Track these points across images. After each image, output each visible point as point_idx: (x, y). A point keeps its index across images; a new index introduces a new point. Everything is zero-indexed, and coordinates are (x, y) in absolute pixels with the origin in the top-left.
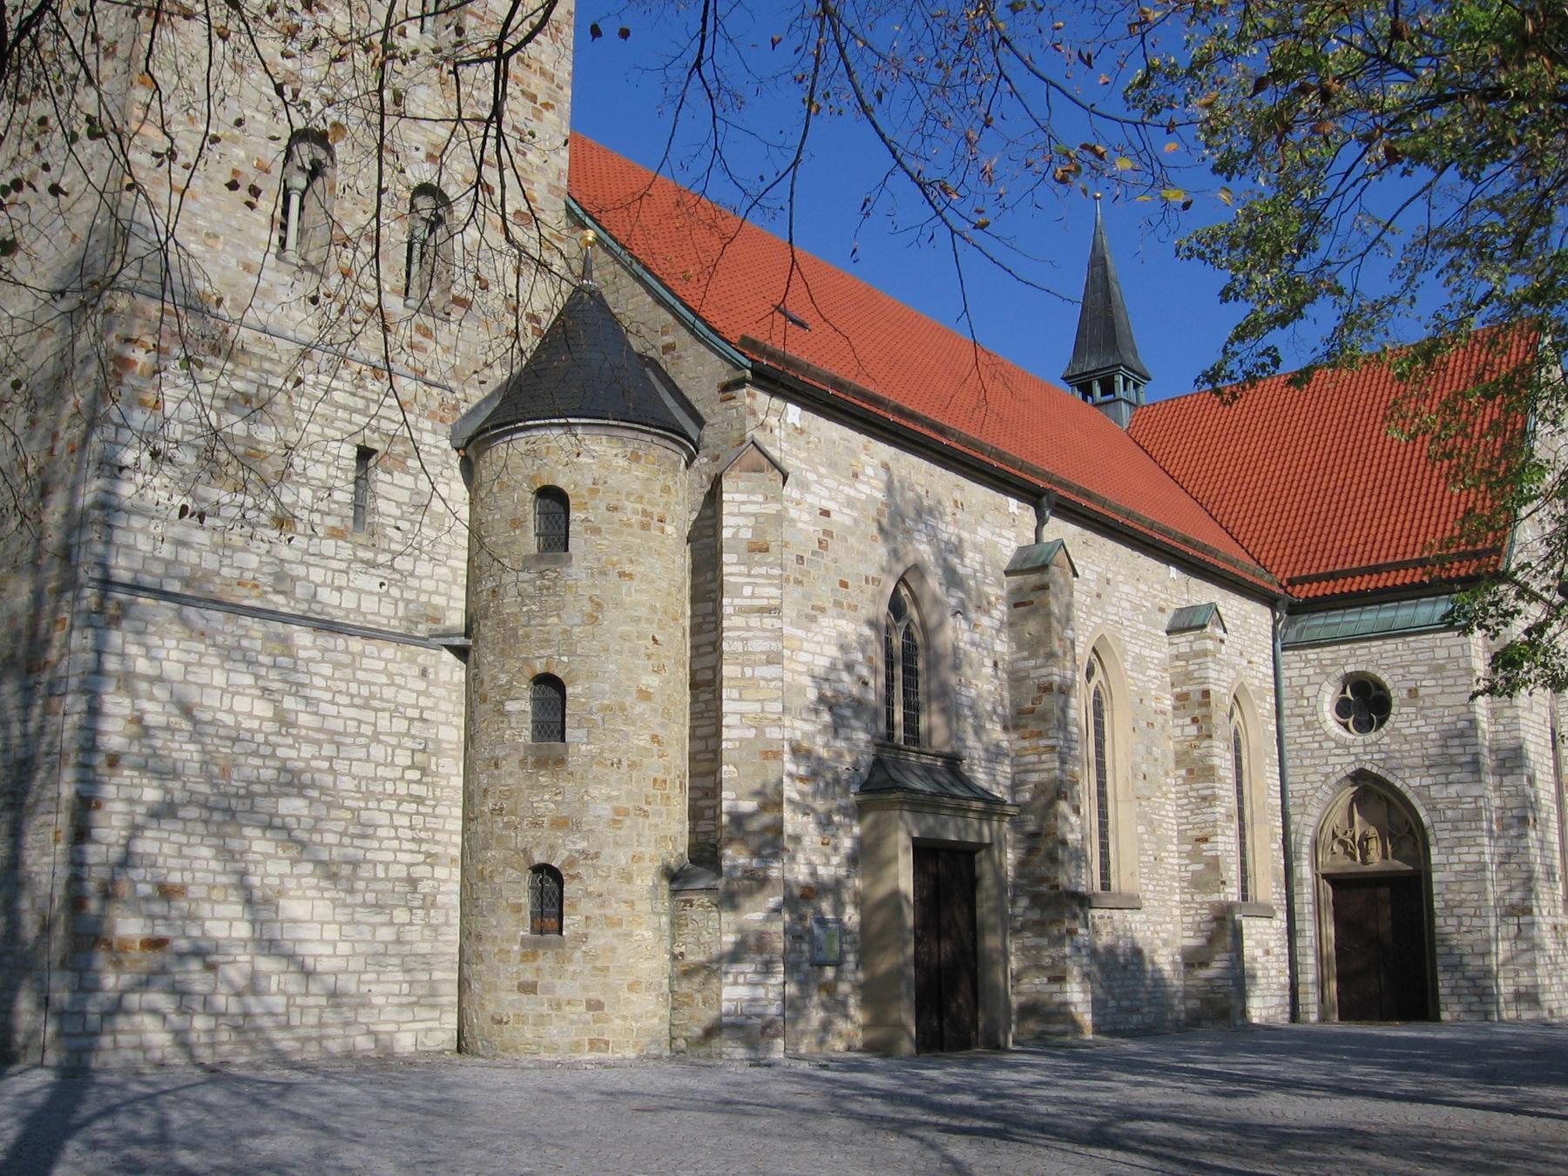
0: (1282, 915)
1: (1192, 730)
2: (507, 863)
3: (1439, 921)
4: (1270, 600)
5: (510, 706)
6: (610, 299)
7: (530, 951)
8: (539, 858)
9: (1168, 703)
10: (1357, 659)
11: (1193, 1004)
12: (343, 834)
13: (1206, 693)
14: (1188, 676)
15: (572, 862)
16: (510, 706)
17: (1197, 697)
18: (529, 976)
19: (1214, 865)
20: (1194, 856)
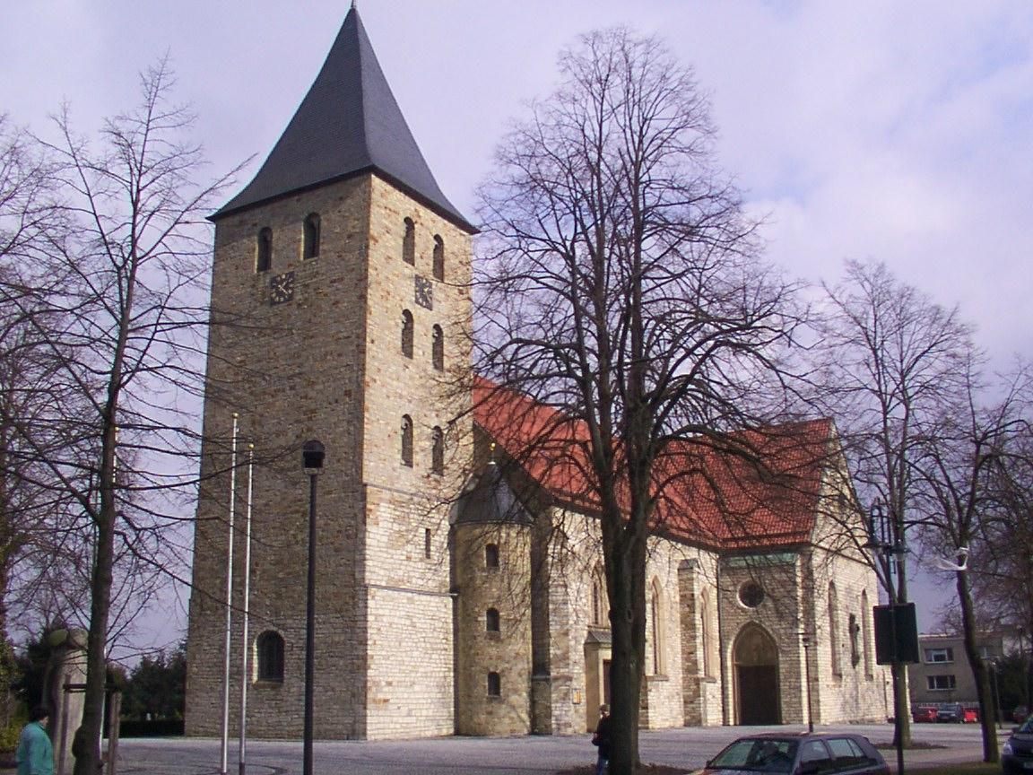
0: (719, 682)
1: (687, 609)
2: (481, 672)
3: (782, 684)
4: (715, 550)
5: (480, 619)
6: (399, 344)
7: (490, 701)
8: (492, 670)
9: (678, 598)
10: (540, 743)
11: (647, 482)
12: (417, 672)
13: (693, 595)
14: (686, 589)
15: (503, 671)
16: (480, 619)
17: (688, 596)
18: (490, 709)
19: (695, 663)
20: (687, 660)
